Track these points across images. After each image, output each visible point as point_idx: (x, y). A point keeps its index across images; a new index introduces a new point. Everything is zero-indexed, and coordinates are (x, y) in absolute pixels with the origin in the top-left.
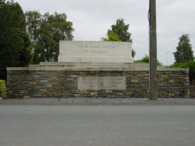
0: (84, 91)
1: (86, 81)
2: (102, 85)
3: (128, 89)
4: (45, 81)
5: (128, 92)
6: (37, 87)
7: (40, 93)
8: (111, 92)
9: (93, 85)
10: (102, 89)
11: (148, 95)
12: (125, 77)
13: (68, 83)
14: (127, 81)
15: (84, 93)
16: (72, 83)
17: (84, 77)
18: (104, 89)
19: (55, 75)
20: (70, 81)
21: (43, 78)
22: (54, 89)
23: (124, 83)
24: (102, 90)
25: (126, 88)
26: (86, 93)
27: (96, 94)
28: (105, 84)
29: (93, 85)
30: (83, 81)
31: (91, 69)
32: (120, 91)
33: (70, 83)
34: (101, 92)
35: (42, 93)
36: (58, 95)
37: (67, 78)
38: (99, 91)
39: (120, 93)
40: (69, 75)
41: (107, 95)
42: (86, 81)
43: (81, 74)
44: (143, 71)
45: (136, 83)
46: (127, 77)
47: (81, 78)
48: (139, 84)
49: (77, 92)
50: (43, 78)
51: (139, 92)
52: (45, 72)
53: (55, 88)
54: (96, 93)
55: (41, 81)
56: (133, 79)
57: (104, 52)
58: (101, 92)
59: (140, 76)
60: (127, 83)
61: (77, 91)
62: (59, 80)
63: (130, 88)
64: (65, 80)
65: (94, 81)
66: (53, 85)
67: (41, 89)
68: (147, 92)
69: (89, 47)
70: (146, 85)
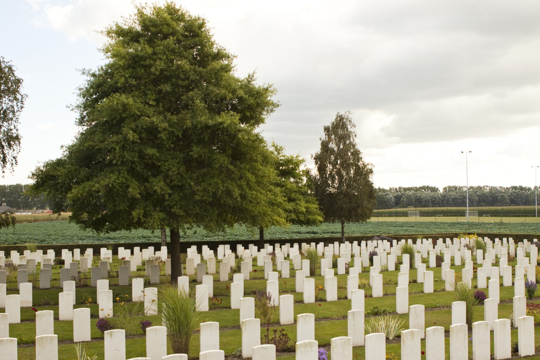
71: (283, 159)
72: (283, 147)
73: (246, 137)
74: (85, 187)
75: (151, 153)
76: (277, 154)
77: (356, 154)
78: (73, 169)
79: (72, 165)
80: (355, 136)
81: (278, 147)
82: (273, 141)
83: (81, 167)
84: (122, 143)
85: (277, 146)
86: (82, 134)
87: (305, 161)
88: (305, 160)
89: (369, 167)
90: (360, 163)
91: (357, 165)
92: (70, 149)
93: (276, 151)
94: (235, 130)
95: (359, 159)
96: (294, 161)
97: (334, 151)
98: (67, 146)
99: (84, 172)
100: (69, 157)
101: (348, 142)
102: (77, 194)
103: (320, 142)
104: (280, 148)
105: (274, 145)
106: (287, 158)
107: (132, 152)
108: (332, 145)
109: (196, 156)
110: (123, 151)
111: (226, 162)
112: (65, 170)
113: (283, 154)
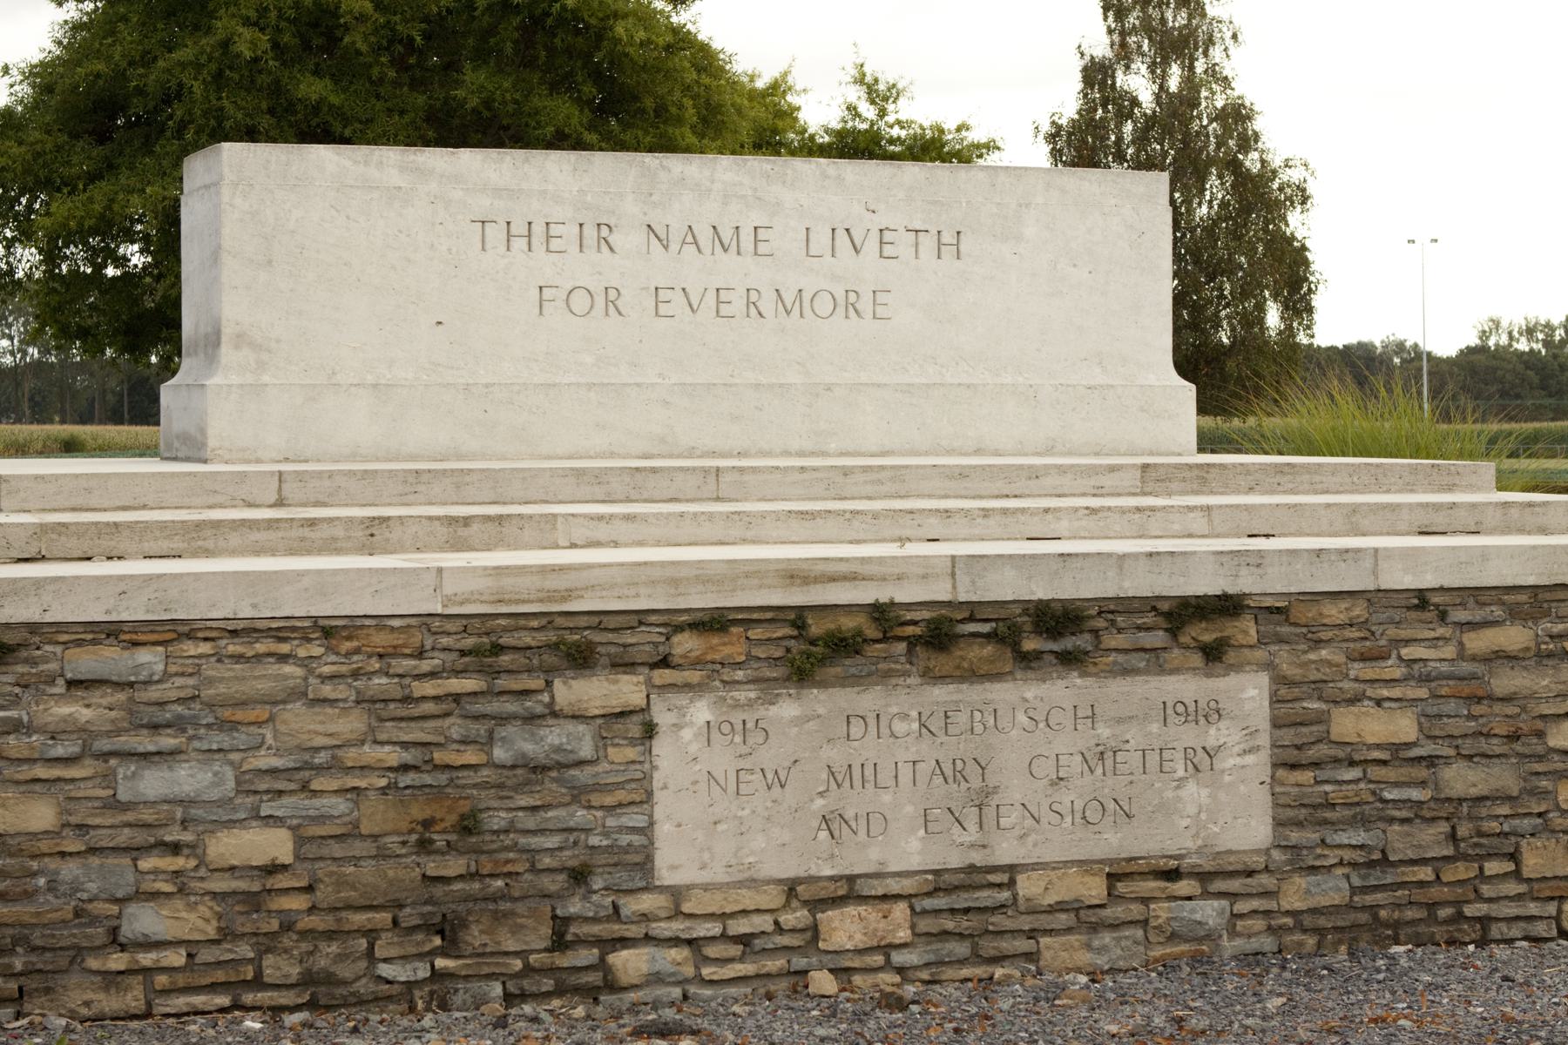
0: (748, 900)
1: (771, 756)
2: (982, 799)
3: (1295, 836)
4: (188, 779)
5: (1300, 881)
6: (69, 870)
7: (117, 961)
8: (1094, 889)
9: (854, 803)
10: (977, 858)
11: (1533, 908)
12: (1264, 679)
13: (524, 801)
14: (1288, 736)
15: (740, 927)
16: (579, 795)
17: (737, 706)
18: (1006, 851)
19: (327, 690)
20: (563, 764)
21: (167, 741)
22: (324, 894)
23: (1250, 759)
24: (973, 879)
25: (1279, 824)
26: (764, 923)
27: (903, 935)
28: (1015, 788)
29: (854, 803)
30: (721, 760)
31: (833, 579)
32: (1204, 877)
33: (551, 788)
34: (961, 900)
35: (147, 959)
36: (385, 970)
37: (503, 719)
38: (941, 883)
39: (1206, 895)
40: (536, 683)
41: (1032, 934)
42: (771, 756)
43: (697, 663)
44: (1477, 594)
45: (1397, 752)
46: (1279, 680)
47: (701, 711)
48: (1431, 761)
49: (645, 917)
50: (155, 727)
51: (1426, 873)
52: (191, 648)
53: (341, 883)
54: (900, 910)
55: (153, 783)
56: (1354, 700)
57: (824, 305)
58: (961, 900)
59: (1437, 656)
60: (1285, 763)
61: (646, 902)
62: (392, 756)
63: (1325, 822)
64: (471, 756)
65: (868, 748)
66: (300, 841)
67: (132, 909)
68: (1517, 875)
69: (628, 239)
70: (1503, 777)
71: (899, 138)
72: (900, 86)
73: (641, 35)
74: (91, 200)
75: (314, 97)
76: (875, 118)
77: (1236, 116)
78: (49, 146)
79: (48, 132)
80: (1235, 37)
81: (882, 87)
82: (859, 61)
83: (75, 136)
84: (213, 66)
85: (876, 81)
86: (76, 27)
87: (999, 149)
88: (999, 144)
89: (1294, 175)
90: (1251, 162)
91: (1234, 166)
92: (36, 75)
93: (873, 102)
94: (601, 15)
95: (1248, 142)
96: (946, 149)
97: (1135, 102)
98: (23, 65)
99: (83, 158)
100: (35, 106)
101: (1200, 67)
102: (67, 219)
103: (1081, 64)
104: (889, 90)
105: (864, 75)
106: (919, 131)
107: (248, 91)
108: (1138, 83)
109: (474, 102)
110: (219, 90)
111: (575, 121)
112: (23, 149)
113: (902, 117)
